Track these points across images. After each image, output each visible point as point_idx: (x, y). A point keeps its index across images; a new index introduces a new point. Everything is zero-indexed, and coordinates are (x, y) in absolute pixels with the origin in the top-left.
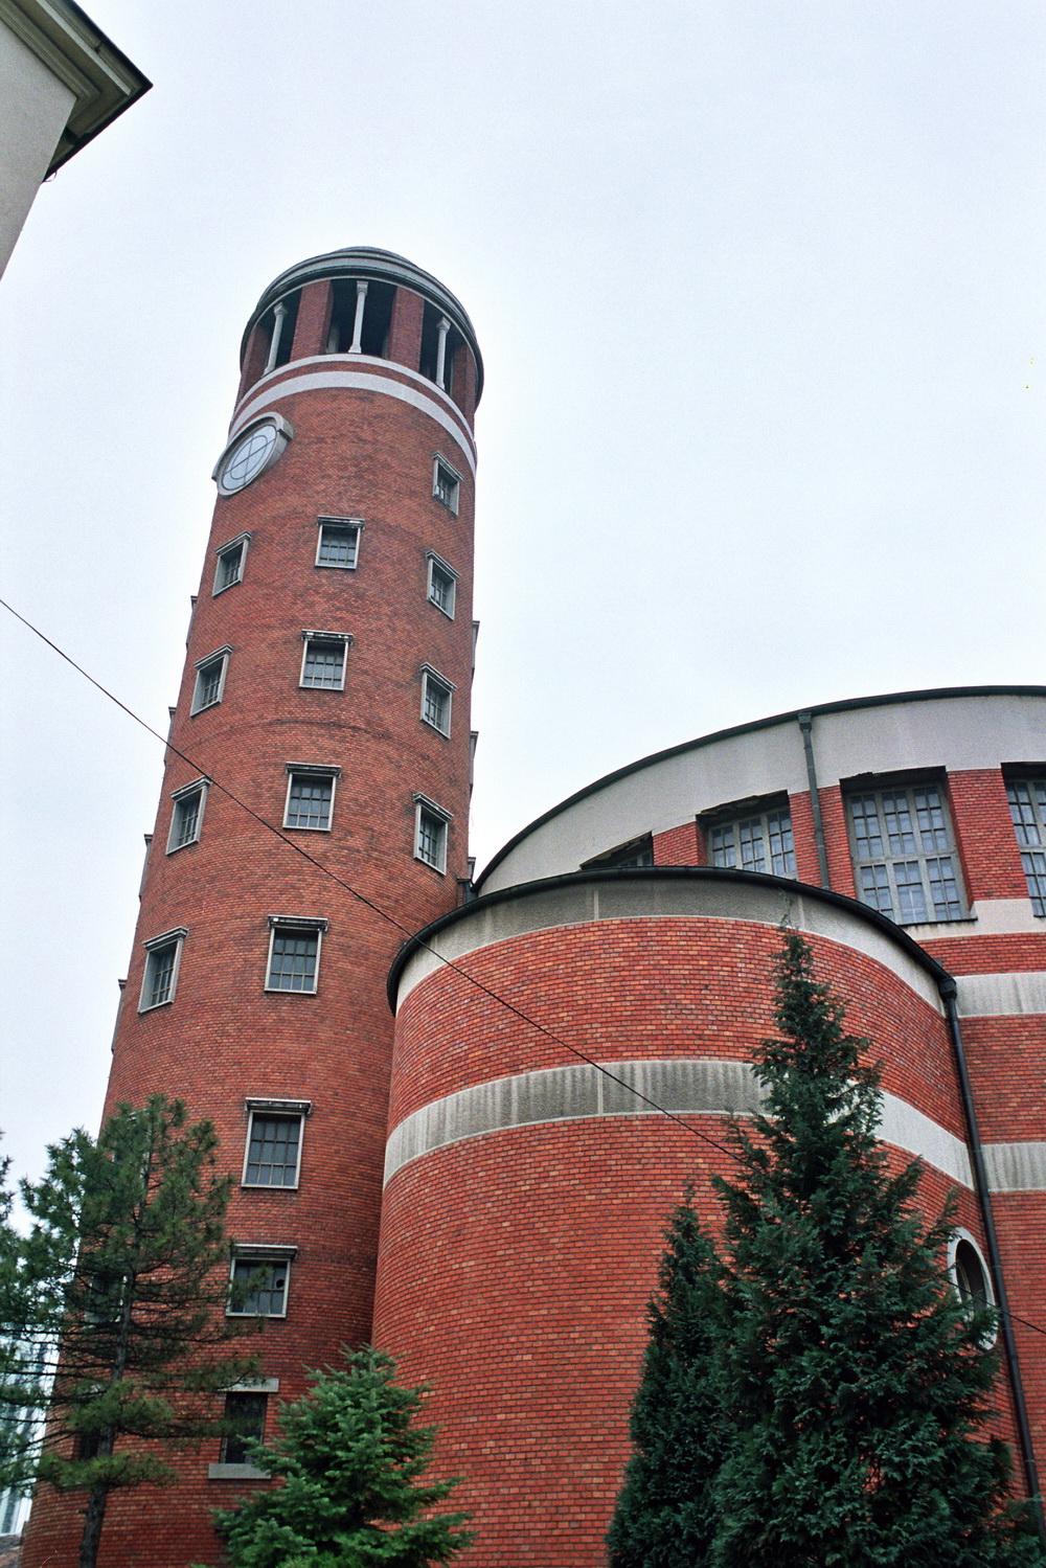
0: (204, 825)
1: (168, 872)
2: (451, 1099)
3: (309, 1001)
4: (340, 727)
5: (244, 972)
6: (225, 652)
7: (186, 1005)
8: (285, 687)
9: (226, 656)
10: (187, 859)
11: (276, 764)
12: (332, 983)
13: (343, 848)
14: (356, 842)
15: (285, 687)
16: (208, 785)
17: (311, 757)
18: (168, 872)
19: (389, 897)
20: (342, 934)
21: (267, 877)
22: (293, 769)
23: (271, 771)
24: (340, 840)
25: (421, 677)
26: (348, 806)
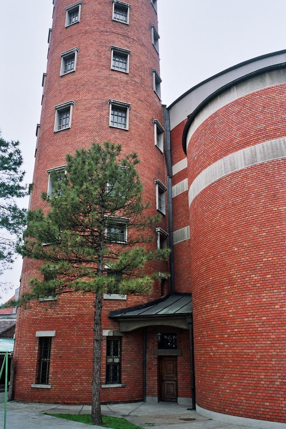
0: (77, 65)
1: (61, 82)
2: (258, 147)
3: (126, 133)
4: (128, 37)
5: (100, 119)
6: (80, 4)
7: (77, 129)
8: (107, 19)
9: (80, 5)
10: (71, 77)
11: (106, 46)
12: (133, 127)
13: (132, 80)
14: (137, 80)
15: (107, 19)
16: (77, 51)
17: (121, 45)
18: (61, 82)
19: (148, 102)
20: (135, 111)
21: (106, 86)
22: (114, 48)
23: (104, 48)
24: (131, 77)
25: (151, 30)
26: (133, 66)
